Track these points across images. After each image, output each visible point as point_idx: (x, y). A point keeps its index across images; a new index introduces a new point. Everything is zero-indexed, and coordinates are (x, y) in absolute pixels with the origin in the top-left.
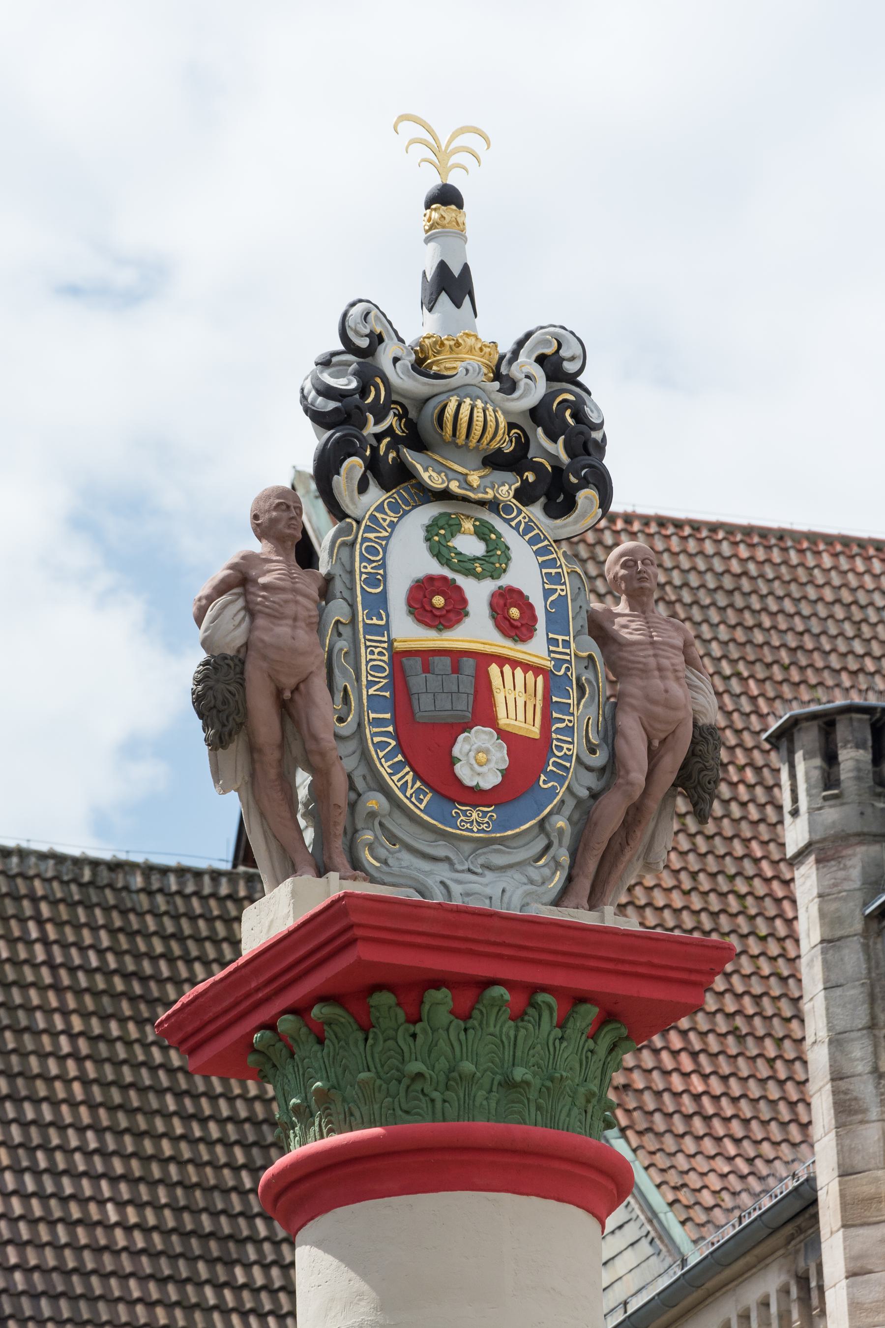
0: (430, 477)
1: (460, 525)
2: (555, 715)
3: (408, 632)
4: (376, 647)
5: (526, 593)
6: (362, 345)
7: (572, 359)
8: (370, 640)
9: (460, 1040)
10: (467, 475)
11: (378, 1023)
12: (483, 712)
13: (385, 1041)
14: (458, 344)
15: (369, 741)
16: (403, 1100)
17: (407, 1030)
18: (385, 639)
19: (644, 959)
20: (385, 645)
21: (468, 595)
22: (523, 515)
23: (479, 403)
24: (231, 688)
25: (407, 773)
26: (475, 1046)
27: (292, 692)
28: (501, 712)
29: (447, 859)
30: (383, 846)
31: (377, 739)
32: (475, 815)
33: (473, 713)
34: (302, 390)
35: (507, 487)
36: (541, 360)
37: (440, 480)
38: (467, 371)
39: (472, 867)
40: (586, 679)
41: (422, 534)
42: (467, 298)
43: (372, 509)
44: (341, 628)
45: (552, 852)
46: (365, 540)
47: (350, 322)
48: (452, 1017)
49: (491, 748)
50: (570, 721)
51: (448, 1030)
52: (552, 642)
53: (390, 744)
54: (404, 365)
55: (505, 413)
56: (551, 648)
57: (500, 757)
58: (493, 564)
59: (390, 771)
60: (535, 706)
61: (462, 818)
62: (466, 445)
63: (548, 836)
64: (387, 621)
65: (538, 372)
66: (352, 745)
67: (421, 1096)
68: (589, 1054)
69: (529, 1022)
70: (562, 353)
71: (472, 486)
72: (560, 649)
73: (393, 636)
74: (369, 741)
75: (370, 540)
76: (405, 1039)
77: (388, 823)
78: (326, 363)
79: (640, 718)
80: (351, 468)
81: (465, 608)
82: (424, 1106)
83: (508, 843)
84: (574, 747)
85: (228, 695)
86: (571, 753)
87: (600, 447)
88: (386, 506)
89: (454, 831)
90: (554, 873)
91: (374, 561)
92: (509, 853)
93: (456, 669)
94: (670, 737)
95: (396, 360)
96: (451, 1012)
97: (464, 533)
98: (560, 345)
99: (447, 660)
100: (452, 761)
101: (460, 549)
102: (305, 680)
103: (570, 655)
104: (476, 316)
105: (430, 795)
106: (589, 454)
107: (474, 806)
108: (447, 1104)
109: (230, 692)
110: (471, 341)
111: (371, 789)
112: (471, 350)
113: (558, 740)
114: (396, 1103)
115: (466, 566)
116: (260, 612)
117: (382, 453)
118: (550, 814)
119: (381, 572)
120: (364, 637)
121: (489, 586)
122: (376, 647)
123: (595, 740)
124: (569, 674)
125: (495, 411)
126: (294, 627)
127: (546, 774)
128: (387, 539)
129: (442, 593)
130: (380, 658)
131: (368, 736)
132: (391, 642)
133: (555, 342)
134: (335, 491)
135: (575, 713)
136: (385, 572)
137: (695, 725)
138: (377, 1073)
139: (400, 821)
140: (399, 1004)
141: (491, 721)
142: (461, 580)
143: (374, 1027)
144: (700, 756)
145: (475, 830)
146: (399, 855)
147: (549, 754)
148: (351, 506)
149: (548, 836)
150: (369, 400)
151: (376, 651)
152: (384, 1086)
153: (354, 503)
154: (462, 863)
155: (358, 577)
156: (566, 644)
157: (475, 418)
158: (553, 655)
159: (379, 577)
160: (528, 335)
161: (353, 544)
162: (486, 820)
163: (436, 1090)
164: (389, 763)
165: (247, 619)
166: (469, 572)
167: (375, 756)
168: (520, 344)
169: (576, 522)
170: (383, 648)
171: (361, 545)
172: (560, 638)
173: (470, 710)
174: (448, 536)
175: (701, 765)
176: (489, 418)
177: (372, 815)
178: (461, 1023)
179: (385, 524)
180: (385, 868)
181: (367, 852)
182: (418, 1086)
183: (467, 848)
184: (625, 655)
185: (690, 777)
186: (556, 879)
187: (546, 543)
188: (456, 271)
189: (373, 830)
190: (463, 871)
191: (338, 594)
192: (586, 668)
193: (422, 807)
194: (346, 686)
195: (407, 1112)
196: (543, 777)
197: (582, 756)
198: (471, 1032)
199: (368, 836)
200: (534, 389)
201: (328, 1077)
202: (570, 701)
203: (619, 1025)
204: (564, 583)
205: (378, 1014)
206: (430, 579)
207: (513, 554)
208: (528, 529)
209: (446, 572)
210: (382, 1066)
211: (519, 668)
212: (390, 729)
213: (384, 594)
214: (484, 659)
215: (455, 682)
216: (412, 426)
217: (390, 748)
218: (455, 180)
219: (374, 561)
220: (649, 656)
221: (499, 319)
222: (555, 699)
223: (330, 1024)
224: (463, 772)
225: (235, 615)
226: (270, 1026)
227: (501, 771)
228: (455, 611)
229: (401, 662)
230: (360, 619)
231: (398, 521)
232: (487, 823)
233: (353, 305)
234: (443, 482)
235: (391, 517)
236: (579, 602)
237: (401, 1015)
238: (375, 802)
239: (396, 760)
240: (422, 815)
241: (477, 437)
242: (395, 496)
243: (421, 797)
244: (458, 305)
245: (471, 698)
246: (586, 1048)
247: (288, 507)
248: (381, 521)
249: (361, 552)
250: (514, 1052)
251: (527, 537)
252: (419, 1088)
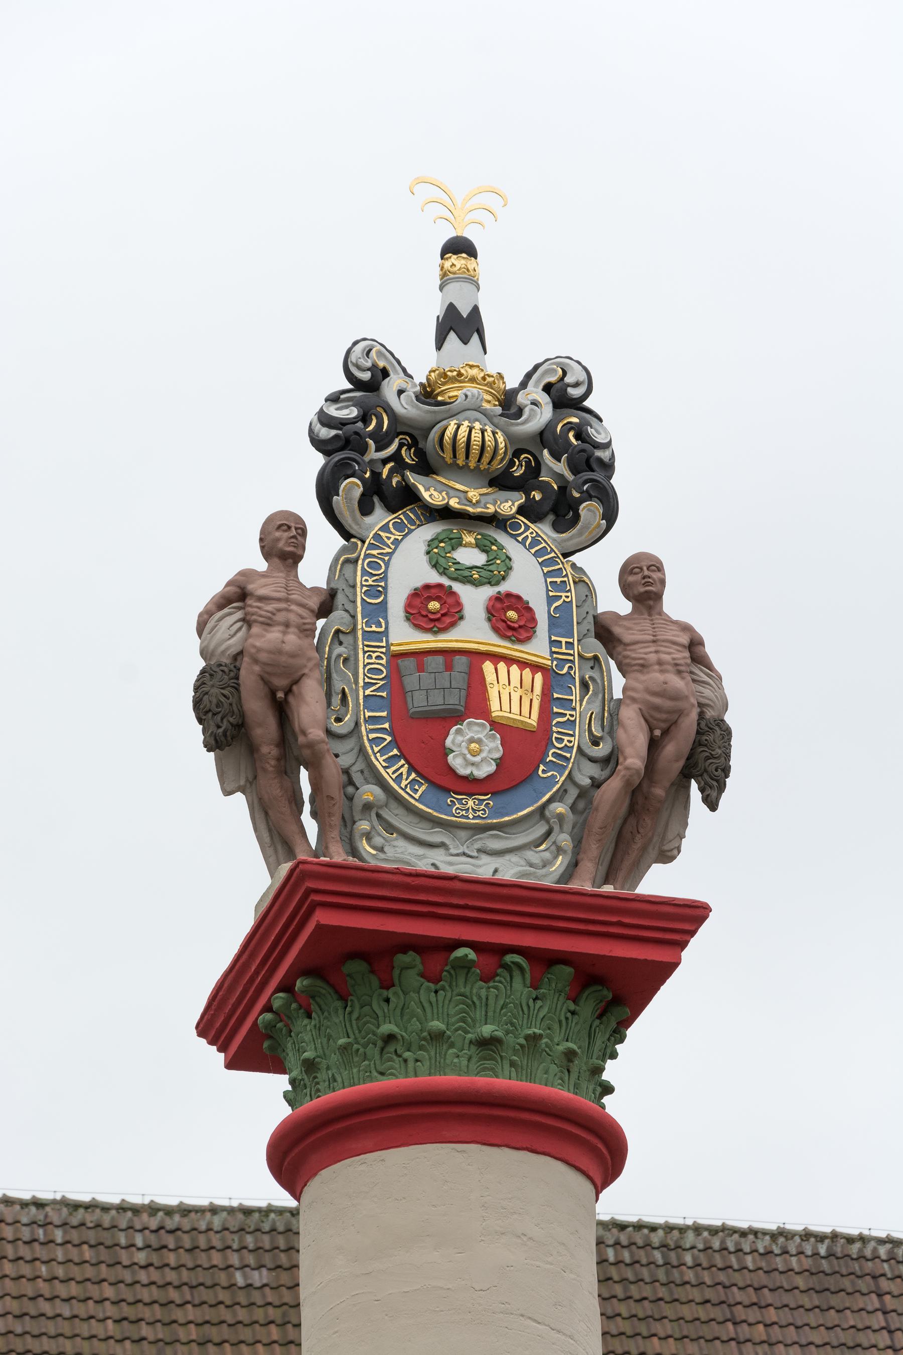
2: (555, 710)
3: (403, 635)
4: (374, 652)
5: (525, 598)
6: (368, 380)
7: (577, 385)
8: (368, 646)
9: (431, 1003)
10: (467, 492)
11: (354, 991)
12: (475, 703)
13: (362, 1007)
14: (460, 374)
15: (365, 738)
16: (378, 1062)
17: (380, 995)
18: (384, 644)
19: (614, 919)
20: (384, 650)
21: (464, 599)
22: (531, 530)
23: (477, 425)
24: (225, 692)
25: (402, 766)
26: (446, 1006)
27: (286, 694)
28: (494, 705)
29: (442, 845)
30: (380, 835)
31: (372, 736)
32: (471, 803)
33: (466, 707)
34: (311, 424)
35: (510, 503)
36: (548, 388)
37: (441, 498)
38: (466, 396)
39: (467, 851)
40: (590, 677)
41: (424, 548)
42: (475, 337)
43: (376, 529)
44: (341, 637)
45: (552, 838)
46: (367, 556)
47: (353, 358)
49: (484, 739)
50: (572, 716)
51: (418, 993)
52: (552, 643)
53: (386, 739)
54: (408, 396)
55: (505, 433)
56: (554, 649)
57: (493, 747)
58: (492, 572)
59: (384, 764)
60: (531, 700)
61: (458, 806)
62: (466, 466)
63: (548, 822)
64: (387, 628)
65: (544, 399)
66: (350, 743)
67: (395, 1057)
68: (569, 1015)
69: (500, 982)
70: (568, 380)
71: (471, 502)
72: (564, 650)
73: (391, 641)
74: (365, 738)
75: (374, 556)
76: (379, 1005)
77: (385, 814)
78: (334, 399)
79: (640, 709)
80: (348, 490)
81: (460, 611)
82: (397, 1066)
83: (506, 830)
84: (576, 739)
85: (223, 699)
86: (572, 744)
87: (608, 467)
88: (391, 526)
89: (449, 818)
90: (556, 857)
91: (376, 575)
92: (506, 838)
93: (449, 667)
94: (672, 728)
95: (400, 392)
96: (422, 975)
97: (465, 546)
98: (565, 373)
99: (440, 659)
100: (446, 752)
101: (458, 560)
102: (297, 682)
103: (573, 655)
104: (485, 353)
105: (423, 788)
106: (593, 471)
107: (470, 795)
108: (419, 1063)
109: (225, 696)
110: (474, 372)
111: (368, 782)
112: (473, 380)
113: (558, 733)
114: (372, 1066)
115: (465, 576)
116: (255, 621)
117: (384, 477)
118: (550, 801)
119: (382, 584)
120: (363, 644)
121: (487, 592)
122: (374, 652)
123: (597, 733)
124: (572, 673)
125: (494, 433)
126: (284, 633)
127: (545, 764)
128: (390, 554)
129: (437, 599)
130: (377, 661)
131: (364, 733)
132: (388, 646)
133: (560, 370)
134: (336, 512)
135: (578, 709)
136: (386, 584)
137: (701, 715)
138: (356, 1039)
139: (396, 812)
140: (372, 972)
141: (483, 712)
142: (457, 587)
143: (352, 995)
144: (706, 745)
145: (471, 816)
146: (395, 843)
147: (550, 746)
148: (355, 527)
149: (548, 822)
150: (371, 428)
151: (374, 655)
152: (362, 1050)
153: (357, 524)
154: (457, 847)
155: (358, 590)
156: (570, 645)
157: (473, 438)
158: (555, 656)
159: (380, 589)
160: (536, 368)
161: (356, 561)
162: (483, 807)
163: (409, 1050)
164: (384, 757)
165: (244, 629)
166: (467, 580)
167: (370, 751)
168: (529, 376)
169: (580, 534)
170: (382, 652)
171: (364, 560)
172: (564, 640)
173: (463, 703)
174: (449, 548)
175: (708, 754)
176: (487, 438)
177: (367, 807)
178: (432, 985)
179: (389, 542)
180: (382, 856)
181: (364, 841)
182: (391, 1048)
183: (463, 834)
184: (628, 653)
185: (696, 765)
186: (559, 862)
187: (553, 555)
188: (465, 312)
189: (370, 821)
190: (457, 855)
191: (340, 606)
192: (592, 668)
193: (417, 796)
194: (344, 689)
195: (382, 1074)
196: (542, 767)
197: (584, 748)
198: (441, 992)
199: (364, 825)
200: (539, 414)
201: (316, 1048)
202: (573, 698)
203: (601, 988)
204: (570, 591)
205: (353, 982)
206: (427, 587)
207: (515, 564)
208: (535, 542)
209: (445, 581)
210: (360, 1032)
212: (386, 726)
213: (384, 603)
214: (478, 656)
215: (448, 679)
216: (421, 454)
217: (385, 743)
218: (470, 233)
219: (376, 575)
220: (651, 652)
221: (509, 355)
222: (556, 695)
223: (313, 997)
224: (455, 761)
225: (232, 626)
226: (268, 1008)
227: (495, 760)
228: (450, 614)
229: (397, 664)
230: (359, 627)
231: (402, 539)
232: (483, 810)
233: (355, 343)
234: (444, 499)
235: (398, 535)
236: (586, 608)
237: (375, 982)
238: (369, 792)
239: (391, 754)
240: (417, 804)
241: (488, 460)
242: (401, 516)
243: (417, 787)
244: (465, 342)
245: (464, 693)
247: (289, 527)
248: (386, 539)
249: (363, 567)
250: (486, 1012)
251: (533, 551)
252: (392, 1050)
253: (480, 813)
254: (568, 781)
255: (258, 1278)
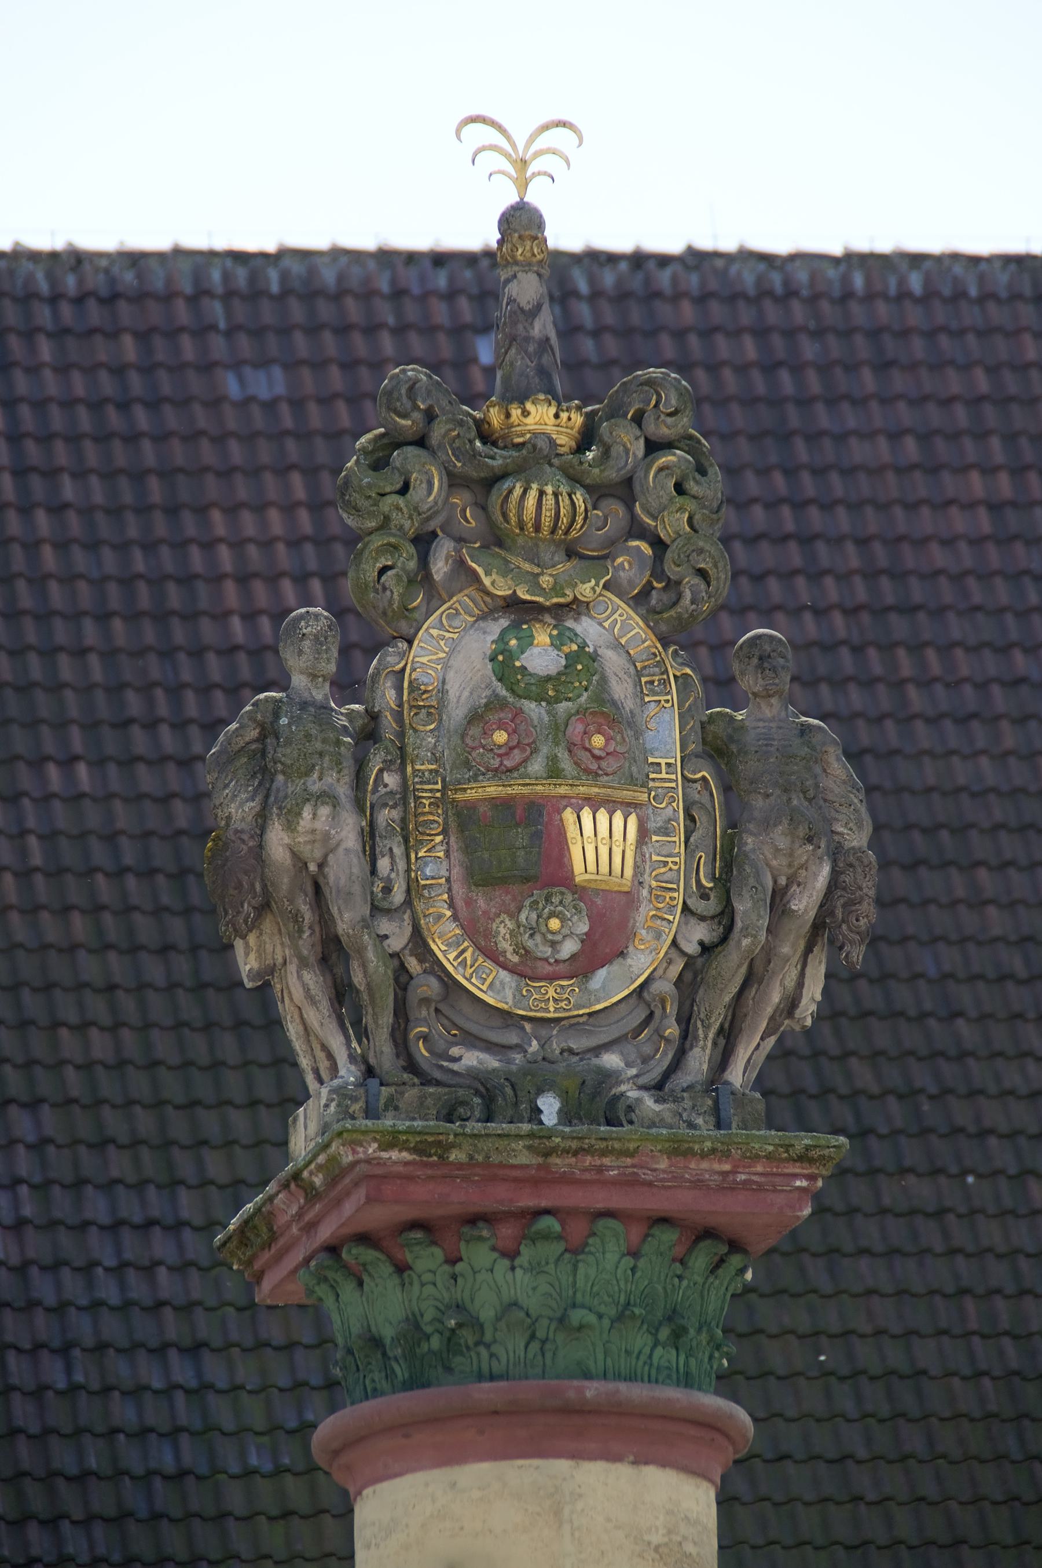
0: (493, 583)
1: (532, 636)
18: (439, 786)
23: (549, 489)
28: (578, 867)
32: (551, 993)
45: (653, 1025)
48: (495, 1255)
59: (443, 948)
60: (624, 852)
68: (676, 1280)
72: (664, 775)
86: (675, 902)
103: (676, 781)
145: (552, 1009)
211: (602, 810)
242: (457, 605)
246: (671, 1274)
253: (563, 1004)
254: (673, 950)
255: (269, 384)
